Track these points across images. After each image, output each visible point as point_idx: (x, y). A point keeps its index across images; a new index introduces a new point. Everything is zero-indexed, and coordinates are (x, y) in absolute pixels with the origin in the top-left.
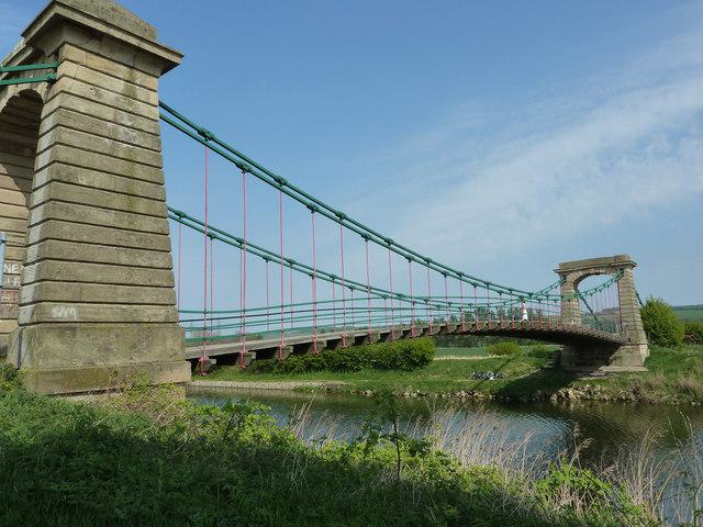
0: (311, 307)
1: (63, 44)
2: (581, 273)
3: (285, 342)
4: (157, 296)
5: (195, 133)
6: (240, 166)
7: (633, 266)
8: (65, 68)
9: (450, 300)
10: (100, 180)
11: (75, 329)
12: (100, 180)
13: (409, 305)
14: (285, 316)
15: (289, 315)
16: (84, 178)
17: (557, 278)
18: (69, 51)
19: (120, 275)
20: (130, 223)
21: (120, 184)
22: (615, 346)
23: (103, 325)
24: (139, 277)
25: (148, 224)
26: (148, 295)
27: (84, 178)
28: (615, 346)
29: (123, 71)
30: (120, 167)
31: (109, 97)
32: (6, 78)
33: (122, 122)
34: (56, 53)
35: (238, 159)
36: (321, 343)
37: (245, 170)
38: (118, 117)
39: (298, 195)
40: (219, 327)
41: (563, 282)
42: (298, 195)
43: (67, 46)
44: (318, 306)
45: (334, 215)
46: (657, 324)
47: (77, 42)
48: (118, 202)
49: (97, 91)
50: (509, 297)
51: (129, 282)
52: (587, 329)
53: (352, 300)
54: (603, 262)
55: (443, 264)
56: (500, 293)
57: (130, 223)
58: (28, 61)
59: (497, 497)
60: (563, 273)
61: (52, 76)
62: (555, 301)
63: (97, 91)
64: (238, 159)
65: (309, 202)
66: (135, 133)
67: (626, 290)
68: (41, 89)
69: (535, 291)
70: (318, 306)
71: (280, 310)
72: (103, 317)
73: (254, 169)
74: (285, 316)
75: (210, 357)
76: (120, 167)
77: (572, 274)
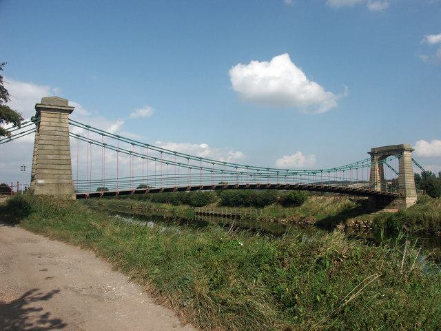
0: (199, 175)
3: (134, 188)
6: (90, 127)
7: (368, 153)
10: (52, 147)
12: (52, 147)
16: (46, 147)
17: (369, 156)
19: (56, 172)
21: (56, 147)
22: (394, 197)
24: (61, 172)
25: (65, 158)
27: (46, 147)
28: (394, 197)
30: (57, 143)
40: (147, 180)
46: (427, 184)
48: (56, 152)
60: (372, 153)
70: (202, 175)
76: (57, 143)
77: (380, 155)
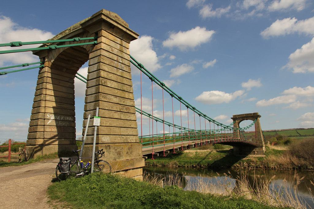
6: (171, 95)
8: (103, 39)
10: (114, 85)
11: (109, 146)
12: (114, 85)
17: (232, 121)
18: (104, 33)
20: (124, 102)
23: (117, 144)
26: (130, 131)
29: (119, 41)
31: (115, 51)
41: (234, 123)
43: (103, 31)
45: (178, 98)
49: (112, 49)
51: (124, 126)
52: (242, 140)
53: (150, 135)
54: (249, 115)
55: (172, 90)
57: (124, 102)
59: (212, 35)
60: (235, 118)
62: (230, 129)
63: (111, 48)
65: (187, 104)
66: (123, 66)
67: (257, 126)
72: (116, 141)
77: (238, 119)
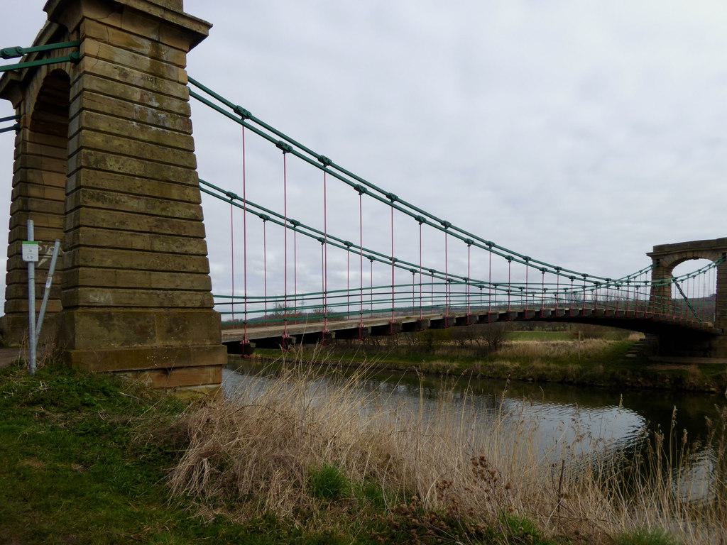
1: (82, 21)
2: (677, 257)
4: (192, 282)
5: (231, 111)
6: (279, 145)
9: (545, 287)
13: (477, 290)
14: (369, 291)
15: (352, 299)
16: (112, 163)
27: (112, 163)
32: (37, 59)
33: (150, 103)
34: (78, 29)
35: (278, 139)
36: (366, 329)
37: (286, 150)
38: (146, 97)
39: (344, 176)
42: (344, 176)
44: (396, 290)
47: (98, 17)
50: (582, 283)
51: (163, 268)
56: (572, 278)
58: (53, 40)
61: (75, 56)
64: (278, 139)
68: (68, 68)
69: (615, 277)
71: (359, 292)
73: (295, 148)
74: (369, 291)
75: (251, 341)
